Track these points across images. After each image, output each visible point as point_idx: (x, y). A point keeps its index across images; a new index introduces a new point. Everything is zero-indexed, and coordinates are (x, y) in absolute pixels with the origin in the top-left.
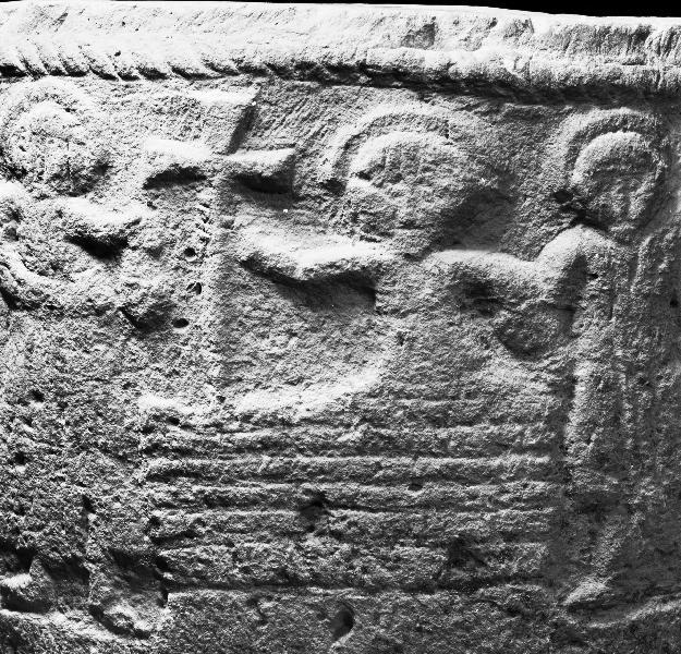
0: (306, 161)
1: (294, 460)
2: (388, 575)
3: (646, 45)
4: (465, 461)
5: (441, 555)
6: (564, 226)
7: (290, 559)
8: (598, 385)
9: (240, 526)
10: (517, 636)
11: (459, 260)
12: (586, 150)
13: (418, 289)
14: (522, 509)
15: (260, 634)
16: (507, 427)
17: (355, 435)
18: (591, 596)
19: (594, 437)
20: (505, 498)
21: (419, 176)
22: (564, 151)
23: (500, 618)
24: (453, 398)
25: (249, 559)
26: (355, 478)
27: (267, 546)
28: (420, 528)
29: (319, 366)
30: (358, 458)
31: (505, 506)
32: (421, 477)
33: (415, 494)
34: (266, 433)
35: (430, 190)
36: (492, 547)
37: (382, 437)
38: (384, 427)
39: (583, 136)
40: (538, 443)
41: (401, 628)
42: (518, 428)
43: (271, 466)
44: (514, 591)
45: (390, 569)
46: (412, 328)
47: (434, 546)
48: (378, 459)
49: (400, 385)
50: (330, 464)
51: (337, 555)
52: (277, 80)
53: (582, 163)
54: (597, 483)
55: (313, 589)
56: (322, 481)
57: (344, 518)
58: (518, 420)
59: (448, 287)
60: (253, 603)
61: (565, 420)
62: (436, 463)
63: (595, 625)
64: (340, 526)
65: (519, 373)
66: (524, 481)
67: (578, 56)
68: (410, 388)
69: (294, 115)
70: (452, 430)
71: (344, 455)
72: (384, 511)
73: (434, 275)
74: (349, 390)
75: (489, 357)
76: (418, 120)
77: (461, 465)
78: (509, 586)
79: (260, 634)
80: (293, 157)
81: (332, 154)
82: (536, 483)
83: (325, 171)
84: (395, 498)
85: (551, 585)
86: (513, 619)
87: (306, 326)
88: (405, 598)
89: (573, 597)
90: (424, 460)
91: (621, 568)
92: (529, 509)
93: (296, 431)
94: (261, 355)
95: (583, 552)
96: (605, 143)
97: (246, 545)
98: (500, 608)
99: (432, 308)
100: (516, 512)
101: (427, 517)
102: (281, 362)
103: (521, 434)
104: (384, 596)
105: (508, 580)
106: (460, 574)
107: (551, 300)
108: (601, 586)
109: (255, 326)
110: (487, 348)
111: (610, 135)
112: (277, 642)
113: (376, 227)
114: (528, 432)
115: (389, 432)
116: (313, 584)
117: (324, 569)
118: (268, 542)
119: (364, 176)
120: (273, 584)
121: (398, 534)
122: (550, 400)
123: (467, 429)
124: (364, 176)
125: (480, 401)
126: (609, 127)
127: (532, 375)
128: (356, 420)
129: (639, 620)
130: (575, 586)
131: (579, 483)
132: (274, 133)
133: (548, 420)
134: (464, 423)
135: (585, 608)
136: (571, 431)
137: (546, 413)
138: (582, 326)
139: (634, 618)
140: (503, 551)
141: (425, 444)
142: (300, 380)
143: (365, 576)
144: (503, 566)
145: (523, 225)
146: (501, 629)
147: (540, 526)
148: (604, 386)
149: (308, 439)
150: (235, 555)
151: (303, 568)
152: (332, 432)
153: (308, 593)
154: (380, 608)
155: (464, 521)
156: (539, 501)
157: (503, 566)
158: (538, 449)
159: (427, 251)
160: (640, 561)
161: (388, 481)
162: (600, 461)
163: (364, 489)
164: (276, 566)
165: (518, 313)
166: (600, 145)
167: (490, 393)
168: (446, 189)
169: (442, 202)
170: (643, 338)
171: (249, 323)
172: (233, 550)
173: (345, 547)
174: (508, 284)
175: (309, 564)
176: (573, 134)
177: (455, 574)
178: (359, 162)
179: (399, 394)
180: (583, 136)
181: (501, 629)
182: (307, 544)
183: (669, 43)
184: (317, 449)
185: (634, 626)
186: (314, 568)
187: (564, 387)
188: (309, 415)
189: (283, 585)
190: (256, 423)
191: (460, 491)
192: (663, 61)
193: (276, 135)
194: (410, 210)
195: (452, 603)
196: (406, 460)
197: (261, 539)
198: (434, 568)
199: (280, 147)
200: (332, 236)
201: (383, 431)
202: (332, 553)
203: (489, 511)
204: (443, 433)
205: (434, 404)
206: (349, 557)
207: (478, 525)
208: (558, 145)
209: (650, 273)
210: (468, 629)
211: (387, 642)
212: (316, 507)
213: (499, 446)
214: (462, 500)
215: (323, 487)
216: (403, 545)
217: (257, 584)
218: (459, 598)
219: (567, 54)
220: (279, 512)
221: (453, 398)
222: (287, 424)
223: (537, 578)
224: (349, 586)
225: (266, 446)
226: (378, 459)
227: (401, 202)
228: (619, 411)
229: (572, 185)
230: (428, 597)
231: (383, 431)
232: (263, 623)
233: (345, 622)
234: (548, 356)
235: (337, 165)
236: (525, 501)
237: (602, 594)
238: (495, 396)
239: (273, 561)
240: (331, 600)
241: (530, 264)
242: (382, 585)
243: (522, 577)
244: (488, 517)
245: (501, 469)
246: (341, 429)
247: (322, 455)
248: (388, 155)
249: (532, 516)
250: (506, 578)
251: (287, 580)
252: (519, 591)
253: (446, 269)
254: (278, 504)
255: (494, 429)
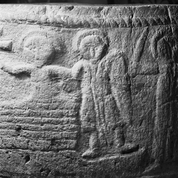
0: (15, 43)
1: (14, 118)
2: (37, 147)
3: (101, 12)
4: (54, 119)
5: (49, 142)
6: (79, 59)
7: (14, 142)
8: (88, 100)
9: (3, 133)
10: (69, 163)
11: (50, 68)
12: (82, 40)
13: (40, 75)
14: (69, 131)
15: (9, 160)
16: (64, 111)
17: (27, 112)
18: (89, 154)
19: (87, 114)
20: (64, 128)
21: (40, 47)
22: (77, 40)
23: (65, 159)
24: (50, 103)
25: (5, 142)
26: (28, 122)
27: (9, 138)
28: (44, 135)
29: (19, 94)
30: (29, 117)
31: (65, 130)
32: (43, 123)
33: (42, 127)
34: (7, 110)
35: (42, 50)
36: (62, 141)
37: (33, 112)
38: (34, 110)
39: (82, 36)
40: (72, 115)
41: (41, 160)
42: (67, 111)
43: (9, 119)
44: (68, 152)
45: (38, 145)
46: (39, 85)
47: (48, 140)
48: (33, 118)
49: (37, 99)
50: (22, 119)
51: (25, 141)
52: (8, 23)
53: (82, 44)
54: (88, 125)
55: (20, 150)
56: (21, 123)
57: (26, 132)
58: (67, 109)
59: (48, 75)
60: (7, 152)
61: (79, 109)
62: (47, 119)
63: (90, 161)
64: (25, 134)
65: (67, 97)
66: (69, 124)
67: (81, 16)
68: (39, 100)
69: (12, 32)
70: (50, 111)
71: (25, 117)
72: (35, 131)
73: (44, 72)
74: (26, 101)
75: (59, 93)
76: (39, 33)
77: (53, 120)
78: (67, 151)
79: (9, 160)
80: (12, 42)
81: (20, 41)
82: (72, 125)
83: (19, 46)
84: (37, 128)
85: (78, 151)
86: (69, 159)
87: (16, 84)
88: (42, 153)
89: (83, 155)
90: (43, 118)
91: (97, 145)
92: (71, 131)
93: (14, 110)
94: (6, 91)
95: (86, 143)
96: (88, 38)
97: (5, 138)
98: (65, 156)
99: (44, 80)
100: (67, 132)
101: (45, 133)
102: (11, 93)
103: (68, 112)
104: (36, 152)
105: (67, 149)
106: (55, 147)
107: (75, 78)
108: (91, 152)
109: (5, 84)
110: (59, 90)
111: (89, 36)
112: (13, 162)
113: (30, 60)
114: (70, 112)
115: (35, 111)
116: (20, 148)
117: (22, 145)
118: (10, 137)
119: (27, 47)
120: (11, 148)
121: (38, 137)
122: (76, 104)
123: (54, 111)
124: (27, 47)
125: (57, 104)
126: (89, 34)
127: (70, 98)
128: (27, 108)
129: (102, 161)
130: (85, 151)
131: (84, 125)
132: (8, 36)
133: (75, 108)
134: (53, 109)
135: (87, 157)
136: (81, 112)
137: (74, 107)
138: (83, 85)
139: (101, 160)
140: (65, 142)
141: (44, 114)
142: (15, 98)
143: (32, 147)
144: (65, 146)
145: (68, 59)
146: (65, 162)
147: (74, 136)
148: (90, 100)
149: (17, 112)
150: (3, 140)
151: (18, 144)
152: (22, 111)
153: (19, 151)
154: (35, 155)
155: (55, 134)
156: (73, 129)
157: (65, 146)
158: (72, 116)
159: (42, 66)
160: (102, 146)
161: (36, 123)
162: (89, 120)
163: (30, 125)
164: (11, 144)
165: (66, 82)
166: (87, 39)
167: (59, 102)
168: (46, 50)
169: (46, 53)
170: (100, 88)
171: (4, 84)
172: (2, 139)
173: (27, 139)
174: (63, 74)
175: (19, 144)
176: (79, 36)
177: (53, 147)
178: (26, 43)
179: (37, 102)
180: (82, 36)
181: (65, 162)
182: (18, 138)
183: (108, 12)
184: (19, 115)
185: (101, 162)
186: (20, 144)
187: (79, 101)
188: (16, 106)
189: (14, 148)
190: (5, 108)
191: (54, 126)
192: (106, 16)
193: (7, 37)
194: (37, 56)
195: (53, 155)
196: (40, 118)
197: (8, 137)
198: (48, 146)
199: (8, 40)
200: (21, 62)
201: (34, 111)
202: (24, 141)
203: (61, 132)
204: (48, 112)
205: (45, 104)
206: (28, 142)
207: (58, 135)
208: (75, 39)
209: (102, 71)
210: (57, 161)
211: (38, 164)
212: (19, 129)
213: (62, 115)
214: (53, 128)
215: (21, 124)
216: (40, 139)
217: (7, 148)
218: (54, 153)
219: (78, 15)
220: (11, 130)
221: (50, 103)
222: (12, 108)
223: (74, 149)
224: (28, 149)
225: (7, 114)
226: (33, 118)
227: (36, 54)
228: (94, 107)
229: (80, 49)
230: (47, 153)
231: (34, 111)
232: (9, 158)
233: (28, 158)
234: (74, 93)
235: (21, 44)
236: (70, 129)
237: (91, 154)
238: (62, 102)
239: (11, 142)
240: (24, 153)
241: (70, 69)
242: (34, 150)
243: (69, 149)
244: (60, 133)
245: (63, 121)
246: (24, 110)
247: (20, 116)
248: (32, 42)
249: (72, 133)
250: (66, 149)
251: (14, 147)
252: (69, 152)
253: (47, 70)
254: (11, 128)
255: (61, 111)
